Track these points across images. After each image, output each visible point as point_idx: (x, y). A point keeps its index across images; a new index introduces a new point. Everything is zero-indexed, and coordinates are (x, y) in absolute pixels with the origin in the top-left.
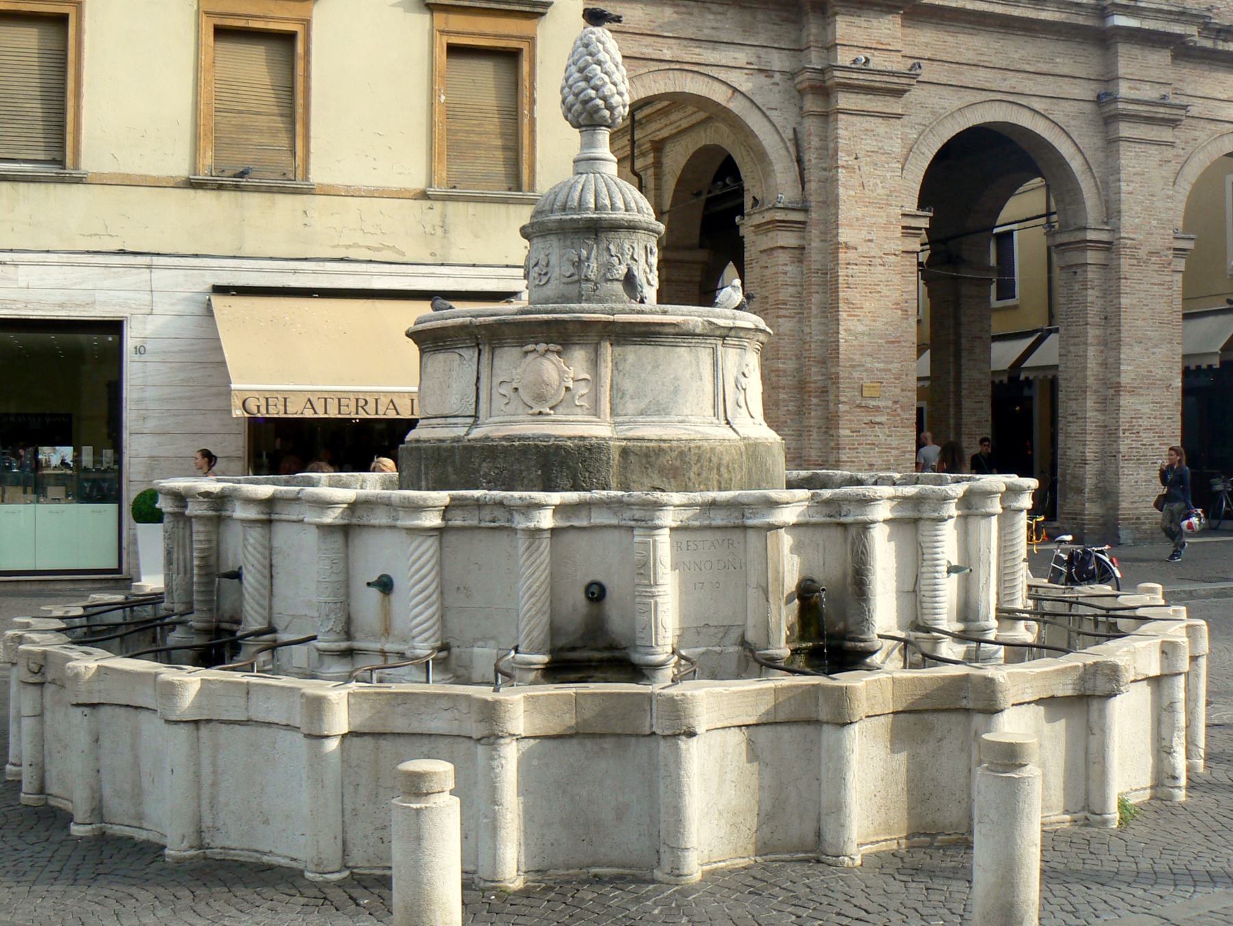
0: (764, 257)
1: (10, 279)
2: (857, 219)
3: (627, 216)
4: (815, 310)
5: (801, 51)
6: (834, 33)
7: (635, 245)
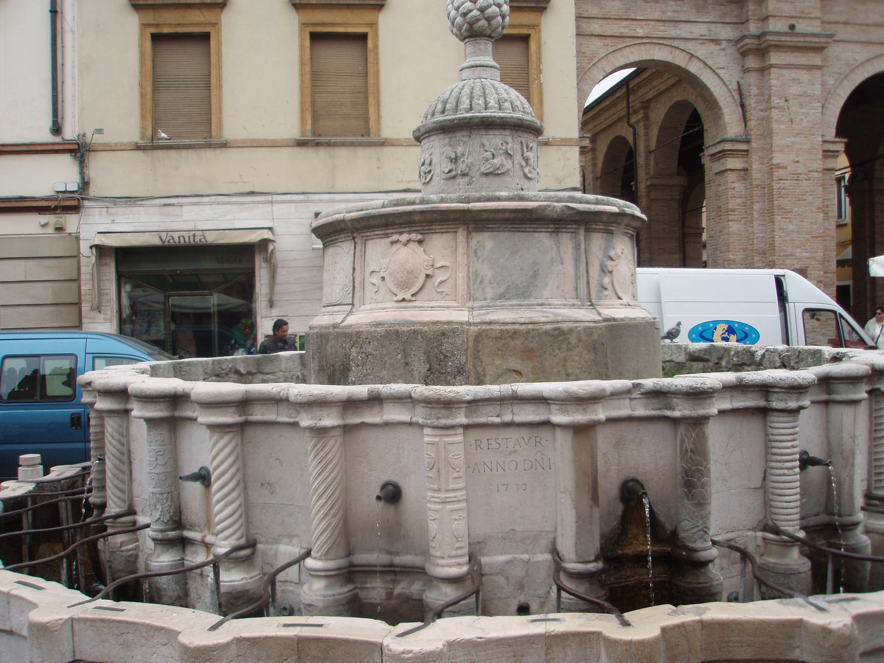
0: (718, 177)
1: (177, 215)
2: (788, 146)
4: (756, 215)
5: (743, 23)
6: (767, 8)
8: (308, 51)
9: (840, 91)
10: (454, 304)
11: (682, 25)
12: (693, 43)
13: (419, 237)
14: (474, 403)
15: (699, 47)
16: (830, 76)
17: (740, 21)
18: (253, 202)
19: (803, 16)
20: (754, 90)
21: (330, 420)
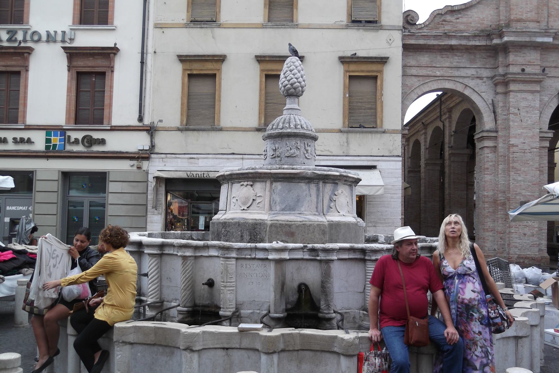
3: (302, 131)
4: (500, 172)
8: (264, 83)
9: (551, 104)
10: (263, 212)
11: (461, 69)
12: (468, 79)
13: (251, 183)
14: (239, 249)
15: (471, 81)
16: (545, 96)
18: (233, 158)
19: (530, 64)
20: (501, 104)
21: (188, 253)
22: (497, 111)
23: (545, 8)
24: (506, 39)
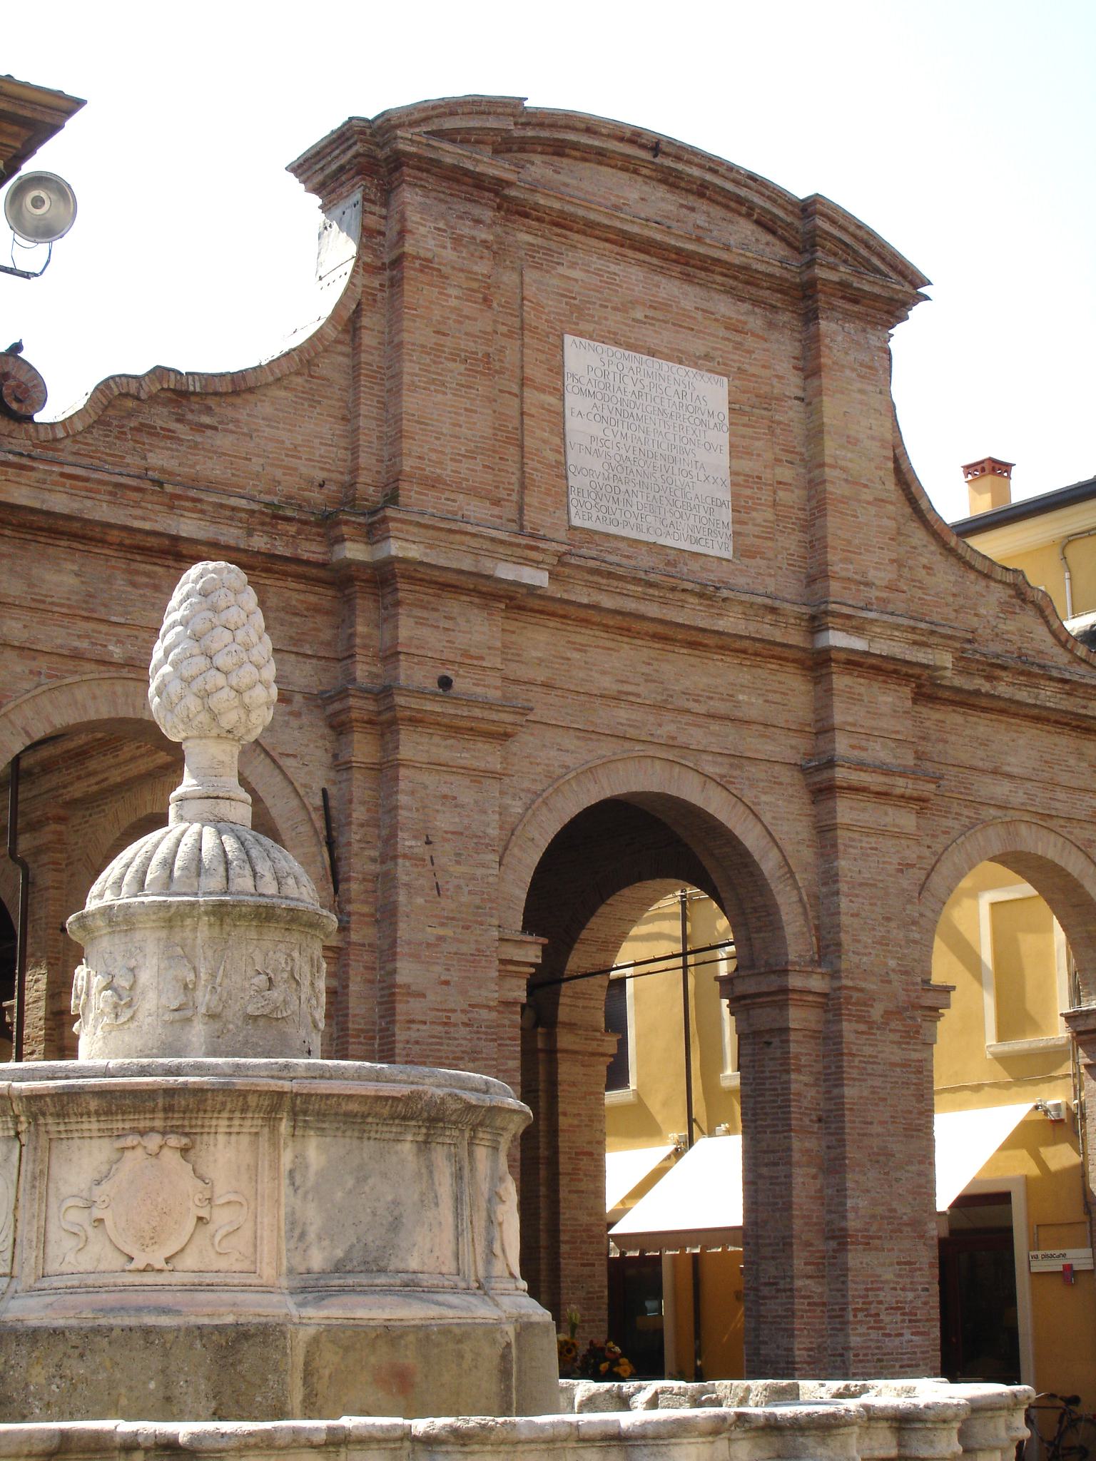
2: (429, 945)
7: (296, 954)
16: (514, 797)
17: (332, 655)
20: (359, 813)
22: (343, 840)
23: (513, 450)
24: (395, 548)
